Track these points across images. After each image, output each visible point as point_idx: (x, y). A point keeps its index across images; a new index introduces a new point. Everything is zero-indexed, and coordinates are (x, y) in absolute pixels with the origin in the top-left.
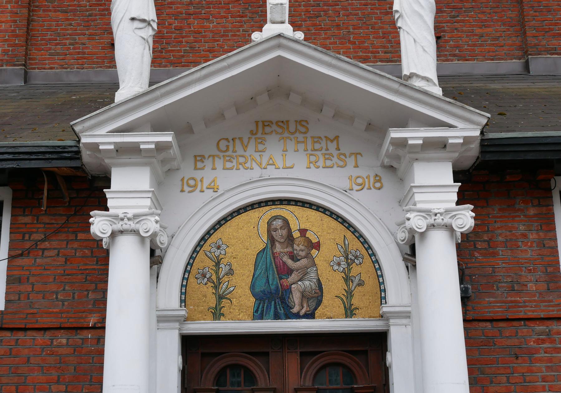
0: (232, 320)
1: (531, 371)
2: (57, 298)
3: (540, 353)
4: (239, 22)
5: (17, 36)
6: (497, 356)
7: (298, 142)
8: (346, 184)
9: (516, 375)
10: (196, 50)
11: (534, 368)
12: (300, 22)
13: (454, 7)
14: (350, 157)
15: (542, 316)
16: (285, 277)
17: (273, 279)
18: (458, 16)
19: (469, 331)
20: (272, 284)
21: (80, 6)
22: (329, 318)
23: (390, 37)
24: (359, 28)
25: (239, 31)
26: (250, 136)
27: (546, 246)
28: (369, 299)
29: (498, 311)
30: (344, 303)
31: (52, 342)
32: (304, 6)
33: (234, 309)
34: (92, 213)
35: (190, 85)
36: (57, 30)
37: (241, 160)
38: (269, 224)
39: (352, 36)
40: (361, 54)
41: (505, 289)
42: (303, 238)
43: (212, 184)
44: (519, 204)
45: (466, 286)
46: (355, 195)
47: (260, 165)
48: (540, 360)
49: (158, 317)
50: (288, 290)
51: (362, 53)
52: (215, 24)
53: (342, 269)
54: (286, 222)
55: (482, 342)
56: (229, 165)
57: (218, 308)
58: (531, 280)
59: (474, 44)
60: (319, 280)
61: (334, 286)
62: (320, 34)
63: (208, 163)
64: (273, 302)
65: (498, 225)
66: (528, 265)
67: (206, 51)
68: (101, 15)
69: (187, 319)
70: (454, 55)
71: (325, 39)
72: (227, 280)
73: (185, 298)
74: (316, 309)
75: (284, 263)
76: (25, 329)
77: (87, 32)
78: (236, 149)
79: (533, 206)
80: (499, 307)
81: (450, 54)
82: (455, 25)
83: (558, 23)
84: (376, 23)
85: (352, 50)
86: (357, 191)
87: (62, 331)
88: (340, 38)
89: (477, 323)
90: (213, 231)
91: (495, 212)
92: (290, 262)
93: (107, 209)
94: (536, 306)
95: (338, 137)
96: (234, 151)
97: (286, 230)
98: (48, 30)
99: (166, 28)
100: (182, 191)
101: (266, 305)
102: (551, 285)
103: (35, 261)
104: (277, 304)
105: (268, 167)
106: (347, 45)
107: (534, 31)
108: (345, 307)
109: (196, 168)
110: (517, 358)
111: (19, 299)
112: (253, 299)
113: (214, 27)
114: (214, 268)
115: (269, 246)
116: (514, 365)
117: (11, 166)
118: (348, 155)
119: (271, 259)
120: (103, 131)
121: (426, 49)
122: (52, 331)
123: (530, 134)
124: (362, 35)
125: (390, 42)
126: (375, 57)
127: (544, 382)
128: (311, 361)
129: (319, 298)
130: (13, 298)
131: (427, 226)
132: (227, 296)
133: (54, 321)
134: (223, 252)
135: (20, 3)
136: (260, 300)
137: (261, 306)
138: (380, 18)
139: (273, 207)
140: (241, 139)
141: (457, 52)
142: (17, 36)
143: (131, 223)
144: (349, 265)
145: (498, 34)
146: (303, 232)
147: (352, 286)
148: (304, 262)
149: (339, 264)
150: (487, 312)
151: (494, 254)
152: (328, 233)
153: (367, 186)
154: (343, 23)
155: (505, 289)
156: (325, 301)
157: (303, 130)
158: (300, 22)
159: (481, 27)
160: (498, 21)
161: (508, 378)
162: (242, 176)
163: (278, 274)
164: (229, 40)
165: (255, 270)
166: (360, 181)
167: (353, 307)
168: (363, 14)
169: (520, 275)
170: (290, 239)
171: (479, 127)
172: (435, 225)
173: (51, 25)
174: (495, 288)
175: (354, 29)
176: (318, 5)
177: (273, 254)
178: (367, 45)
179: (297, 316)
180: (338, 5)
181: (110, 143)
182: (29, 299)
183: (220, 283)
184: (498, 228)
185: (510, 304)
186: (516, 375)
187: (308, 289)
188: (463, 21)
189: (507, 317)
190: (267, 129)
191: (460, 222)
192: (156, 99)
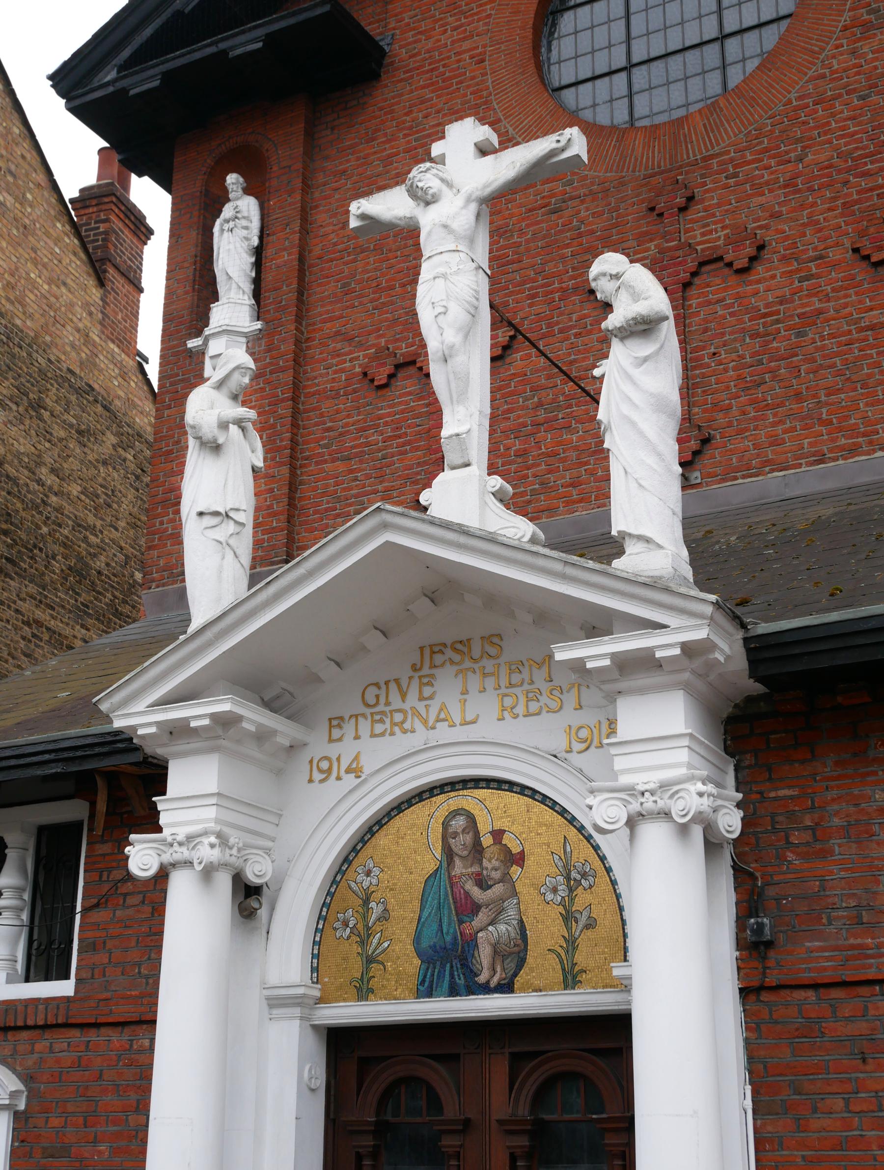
0: (386, 999)
2: (139, 972)
5: (275, 514)
6: (827, 1058)
7: (485, 675)
8: (559, 743)
9: (863, 1095)
10: (551, 487)
12: (727, 402)
14: (568, 692)
16: (468, 919)
17: (449, 924)
19: (774, 1009)
20: (447, 933)
21: (368, 444)
22: (536, 991)
26: (411, 673)
28: (604, 953)
30: (561, 962)
31: (131, 1046)
32: (735, 369)
33: (388, 980)
34: (132, 837)
35: (256, 613)
36: (336, 492)
37: (398, 717)
38: (445, 825)
39: (824, 410)
40: (843, 441)
41: (843, 921)
42: (498, 846)
43: (354, 766)
44: (876, 748)
45: (760, 920)
46: (576, 759)
47: (425, 722)
49: (268, 999)
50: (471, 942)
51: (846, 439)
52: (581, 433)
53: (559, 898)
54: (472, 820)
55: (797, 1029)
56: (379, 728)
57: (365, 980)
60: (521, 922)
61: (546, 931)
62: (764, 418)
63: (349, 728)
64: (448, 965)
65: (830, 795)
67: (567, 487)
68: (401, 453)
69: (320, 1000)
71: (774, 424)
72: (379, 929)
73: (318, 963)
74: (515, 975)
75: (467, 894)
76: (96, 1025)
77: (380, 487)
78: (391, 699)
80: (828, 959)
84: (870, 376)
85: (826, 437)
86: (579, 753)
87: (145, 1026)
88: (803, 419)
89: (788, 992)
90: (361, 845)
91: (829, 769)
92: (476, 892)
93: (159, 830)
96: (388, 704)
97: (471, 834)
98: (324, 494)
99: (502, 456)
100: (311, 781)
101: (436, 970)
103: (114, 915)
104: (455, 968)
105: (439, 725)
106: (817, 428)
108: (563, 970)
109: (331, 740)
110: (864, 1060)
111: (92, 977)
112: (417, 962)
113: (580, 439)
114: (361, 910)
115: (445, 864)
116: (861, 1075)
117: (54, 771)
119: (446, 888)
120: (141, 705)
121: (643, 483)
122: (133, 1027)
123: (834, 616)
124: (844, 404)
128: (531, 1065)
129: (522, 955)
130: (84, 976)
131: (628, 817)
132: (379, 958)
133: (133, 1010)
134: (374, 881)
135: (278, 459)
136: (428, 963)
137: (429, 974)
139: (452, 794)
140: (397, 681)
142: (275, 514)
143: (184, 849)
144: (571, 890)
146: (498, 835)
147: (576, 929)
148: (498, 890)
149: (555, 890)
150: (804, 970)
151: (825, 853)
152: (538, 834)
153: (596, 742)
154: (807, 388)
155: (843, 921)
156: (530, 959)
157: (492, 651)
158: (727, 402)
161: (847, 1101)
162: (400, 744)
163: (457, 914)
165: (422, 910)
166: (584, 734)
167: (577, 969)
168: (845, 362)
169: (876, 893)
170: (477, 849)
171: (705, 621)
172: (644, 813)
173: (327, 486)
174: (824, 921)
176: (760, 363)
177: (450, 878)
178: (853, 421)
179: (486, 989)
180: (797, 355)
181: (149, 724)
182: (104, 976)
183: (369, 936)
184: (833, 800)
185: (849, 953)
186: (863, 1095)
187: (504, 939)
189: (844, 977)
190: (439, 659)
191: (681, 804)
192: (210, 644)
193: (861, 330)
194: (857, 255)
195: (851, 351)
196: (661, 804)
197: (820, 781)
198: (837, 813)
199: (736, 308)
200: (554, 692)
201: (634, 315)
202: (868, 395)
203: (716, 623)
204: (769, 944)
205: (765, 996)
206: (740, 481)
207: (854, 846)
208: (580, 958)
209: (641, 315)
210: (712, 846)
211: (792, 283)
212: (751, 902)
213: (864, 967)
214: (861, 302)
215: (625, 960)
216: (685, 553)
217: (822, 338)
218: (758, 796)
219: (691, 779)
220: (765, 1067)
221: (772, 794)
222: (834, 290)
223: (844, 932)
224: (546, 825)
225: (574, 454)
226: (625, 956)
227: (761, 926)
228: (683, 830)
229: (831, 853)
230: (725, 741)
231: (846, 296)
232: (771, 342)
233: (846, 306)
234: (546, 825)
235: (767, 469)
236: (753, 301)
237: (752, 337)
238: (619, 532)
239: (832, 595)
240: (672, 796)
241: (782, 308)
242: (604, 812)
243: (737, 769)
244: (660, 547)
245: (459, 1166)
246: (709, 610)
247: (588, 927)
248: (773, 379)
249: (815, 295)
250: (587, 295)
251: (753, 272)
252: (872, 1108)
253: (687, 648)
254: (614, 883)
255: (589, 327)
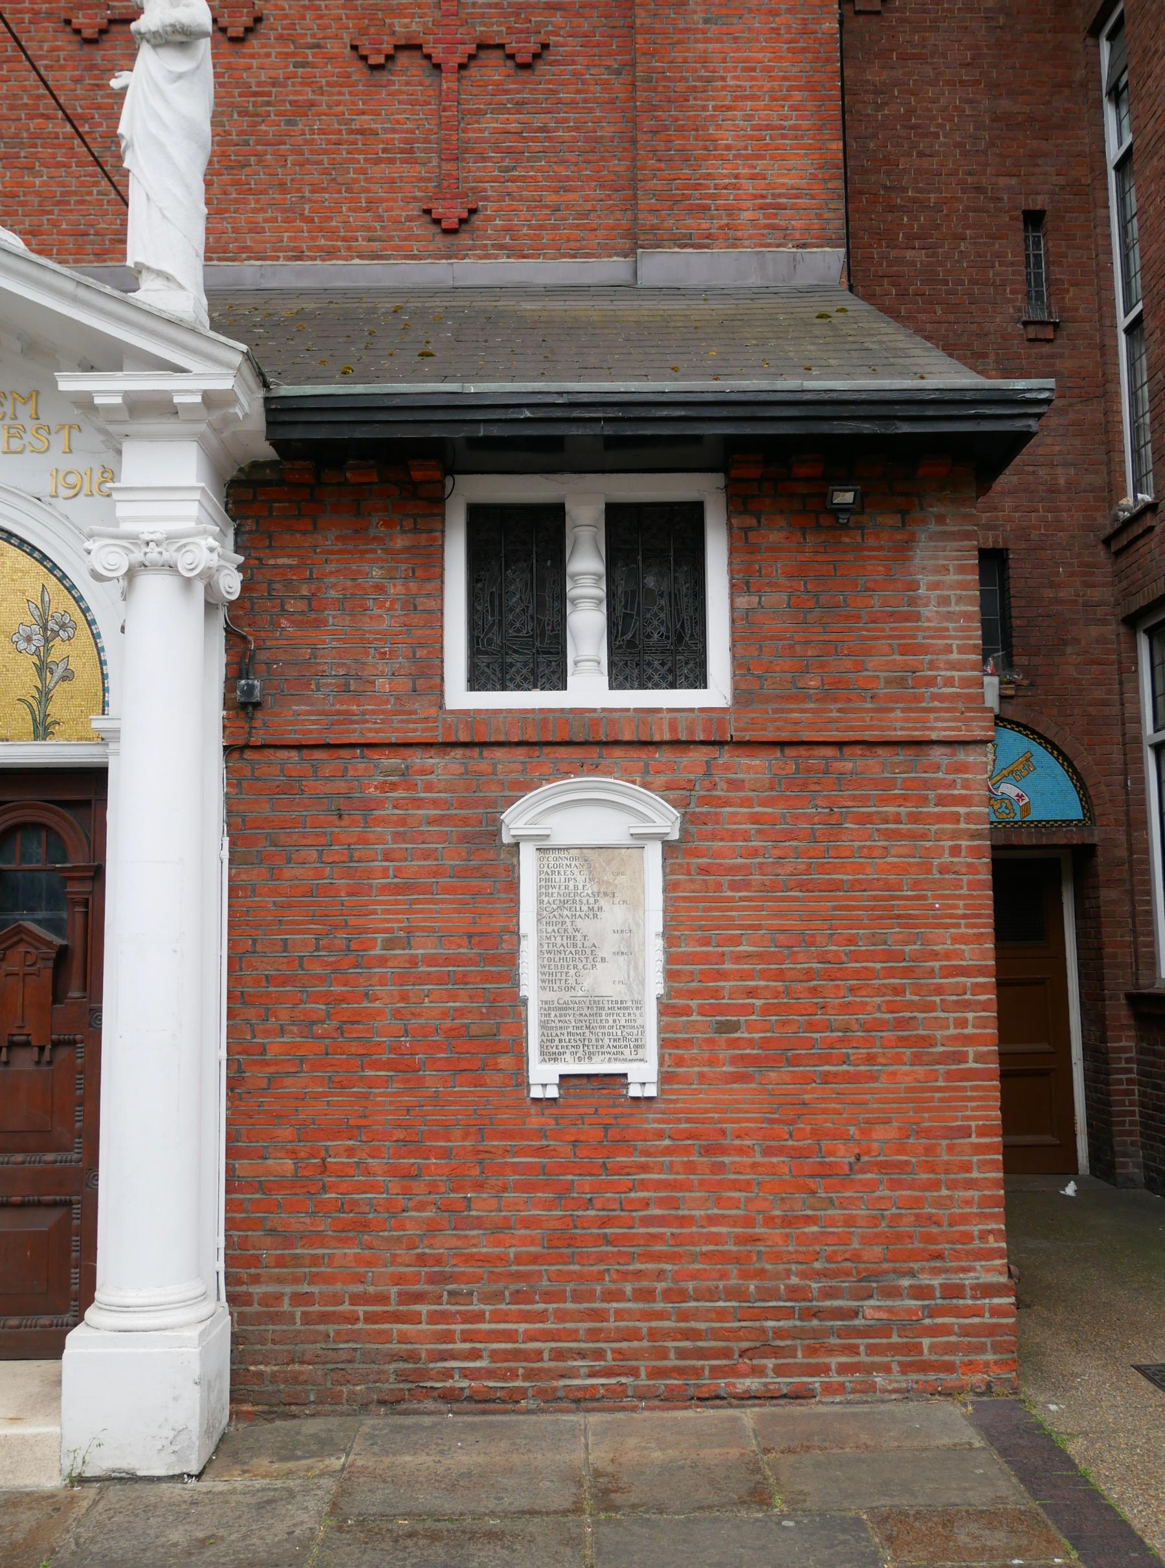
1: (366, 842)
3: (384, 808)
4: (91, 176)
8: (44, 486)
11: (371, 836)
13: (509, 151)
15: (393, 740)
18: (514, 168)
23: (380, 210)
24: (323, 190)
25: (90, 193)
27: (420, 608)
29: (311, 728)
30: (32, 712)
39: (307, 207)
40: (323, 242)
41: (331, 688)
45: (250, 682)
48: (384, 821)
51: (326, 240)
52: (45, 178)
53: (33, 648)
58: (382, 672)
59: (541, 226)
62: (245, 202)
65: (333, 567)
66: (381, 644)
70: (502, 247)
79: (404, 532)
80: (313, 722)
81: (493, 245)
82: (507, 188)
83: (700, 184)
84: (355, 181)
85: (306, 234)
88: (284, 211)
89: (272, 751)
94: (383, 722)
95: (38, 393)
102: (420, 683)
106: (298, 223)
107: (653, 201)
108: (34, 720)
110: (340, 816)
113: (44, 184)
118: (53, 429)
121: (167, 214)
123: (360, 389)
125: (380, 219)
126: (349, 248)
127: (386, 860)
138: (363, 171)
141: (508, 240)
144: (47, 640)
145: (588, 206)
147: (50, 680)
149: (29, 639)
150: (290, 732)
151: (319, 623)
153: (86, 490)
154: (292, 180)
155: (331, 688)
159: (556, 191)
160: (590, 178)
161: (320, 853)
164: (71, 211)
166: (72, 479)
167: (49, 720)
168: (332, 162)
169: (363, 664)
171: (231, 371)
172: (147, 563)
175: (312, 191)
176: (247, 143)
178: (334, 224)
180: (285, 144)
184: (332, 573)
188: (523, 179)
189: (328, 740)
191: (189, 558)
193: (351, 132)
194: (354, 53)
195: (338, 152)
196: (166, 556)
197: (320, 553)
198: (334, 585)
199: (226, 79)
200: (40, 431)
201: (172, 21)
202: (351, 200)
203: (241, 375)
204: (257, 705)
205: (248, 754)
206: (215, 263)
207: (348, 618)
208: (53, 710)
209: (180, 23)
210: (210, 607)
211: (286, 67)
212: (240, 665)
213: (348, 731)
214: (354, 103)
215: (103, 714)
216: (205, 301)
217: (312, 132)
218: (257, 562)
219: (205, 532)
220: (243, 820)
221: (271, 562)
222: (328, 84)
223: (331, 698)
224: (22, 571)
225: (36, 200)
226: (104, 710)
227: (251, 688)
228: (188, 582)
229: (326, 623)
230: (226, 504)
231: (340, 93)
232: (260, 124)
233: (339, 103)
234: (22, 571)
235: (244, 255)
236: (245, 75)
237: (239, 114)
238: (136, 264)
239: (345, 373)
240: (179, 549)
241: (274, 90)
242: (91, 558)
243: (237, 533)
244: (181, 287)
245: (87, 913)
246: (238, 359)
247: (64, 678)
248: (259, 162)
249: (309, 85)
250: (62, 24)
251: (247, 44)
252: (343, 859)
253: (207, 395)
254: (96, 636)
255: (62, 62)
